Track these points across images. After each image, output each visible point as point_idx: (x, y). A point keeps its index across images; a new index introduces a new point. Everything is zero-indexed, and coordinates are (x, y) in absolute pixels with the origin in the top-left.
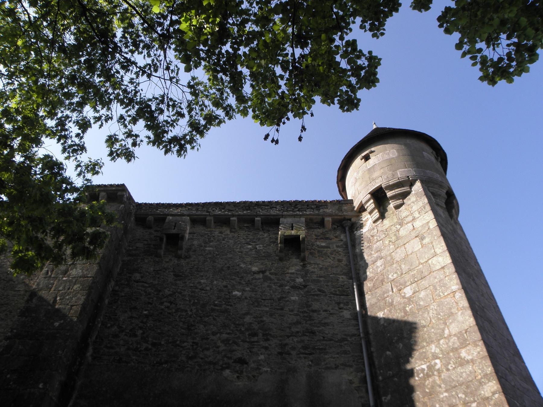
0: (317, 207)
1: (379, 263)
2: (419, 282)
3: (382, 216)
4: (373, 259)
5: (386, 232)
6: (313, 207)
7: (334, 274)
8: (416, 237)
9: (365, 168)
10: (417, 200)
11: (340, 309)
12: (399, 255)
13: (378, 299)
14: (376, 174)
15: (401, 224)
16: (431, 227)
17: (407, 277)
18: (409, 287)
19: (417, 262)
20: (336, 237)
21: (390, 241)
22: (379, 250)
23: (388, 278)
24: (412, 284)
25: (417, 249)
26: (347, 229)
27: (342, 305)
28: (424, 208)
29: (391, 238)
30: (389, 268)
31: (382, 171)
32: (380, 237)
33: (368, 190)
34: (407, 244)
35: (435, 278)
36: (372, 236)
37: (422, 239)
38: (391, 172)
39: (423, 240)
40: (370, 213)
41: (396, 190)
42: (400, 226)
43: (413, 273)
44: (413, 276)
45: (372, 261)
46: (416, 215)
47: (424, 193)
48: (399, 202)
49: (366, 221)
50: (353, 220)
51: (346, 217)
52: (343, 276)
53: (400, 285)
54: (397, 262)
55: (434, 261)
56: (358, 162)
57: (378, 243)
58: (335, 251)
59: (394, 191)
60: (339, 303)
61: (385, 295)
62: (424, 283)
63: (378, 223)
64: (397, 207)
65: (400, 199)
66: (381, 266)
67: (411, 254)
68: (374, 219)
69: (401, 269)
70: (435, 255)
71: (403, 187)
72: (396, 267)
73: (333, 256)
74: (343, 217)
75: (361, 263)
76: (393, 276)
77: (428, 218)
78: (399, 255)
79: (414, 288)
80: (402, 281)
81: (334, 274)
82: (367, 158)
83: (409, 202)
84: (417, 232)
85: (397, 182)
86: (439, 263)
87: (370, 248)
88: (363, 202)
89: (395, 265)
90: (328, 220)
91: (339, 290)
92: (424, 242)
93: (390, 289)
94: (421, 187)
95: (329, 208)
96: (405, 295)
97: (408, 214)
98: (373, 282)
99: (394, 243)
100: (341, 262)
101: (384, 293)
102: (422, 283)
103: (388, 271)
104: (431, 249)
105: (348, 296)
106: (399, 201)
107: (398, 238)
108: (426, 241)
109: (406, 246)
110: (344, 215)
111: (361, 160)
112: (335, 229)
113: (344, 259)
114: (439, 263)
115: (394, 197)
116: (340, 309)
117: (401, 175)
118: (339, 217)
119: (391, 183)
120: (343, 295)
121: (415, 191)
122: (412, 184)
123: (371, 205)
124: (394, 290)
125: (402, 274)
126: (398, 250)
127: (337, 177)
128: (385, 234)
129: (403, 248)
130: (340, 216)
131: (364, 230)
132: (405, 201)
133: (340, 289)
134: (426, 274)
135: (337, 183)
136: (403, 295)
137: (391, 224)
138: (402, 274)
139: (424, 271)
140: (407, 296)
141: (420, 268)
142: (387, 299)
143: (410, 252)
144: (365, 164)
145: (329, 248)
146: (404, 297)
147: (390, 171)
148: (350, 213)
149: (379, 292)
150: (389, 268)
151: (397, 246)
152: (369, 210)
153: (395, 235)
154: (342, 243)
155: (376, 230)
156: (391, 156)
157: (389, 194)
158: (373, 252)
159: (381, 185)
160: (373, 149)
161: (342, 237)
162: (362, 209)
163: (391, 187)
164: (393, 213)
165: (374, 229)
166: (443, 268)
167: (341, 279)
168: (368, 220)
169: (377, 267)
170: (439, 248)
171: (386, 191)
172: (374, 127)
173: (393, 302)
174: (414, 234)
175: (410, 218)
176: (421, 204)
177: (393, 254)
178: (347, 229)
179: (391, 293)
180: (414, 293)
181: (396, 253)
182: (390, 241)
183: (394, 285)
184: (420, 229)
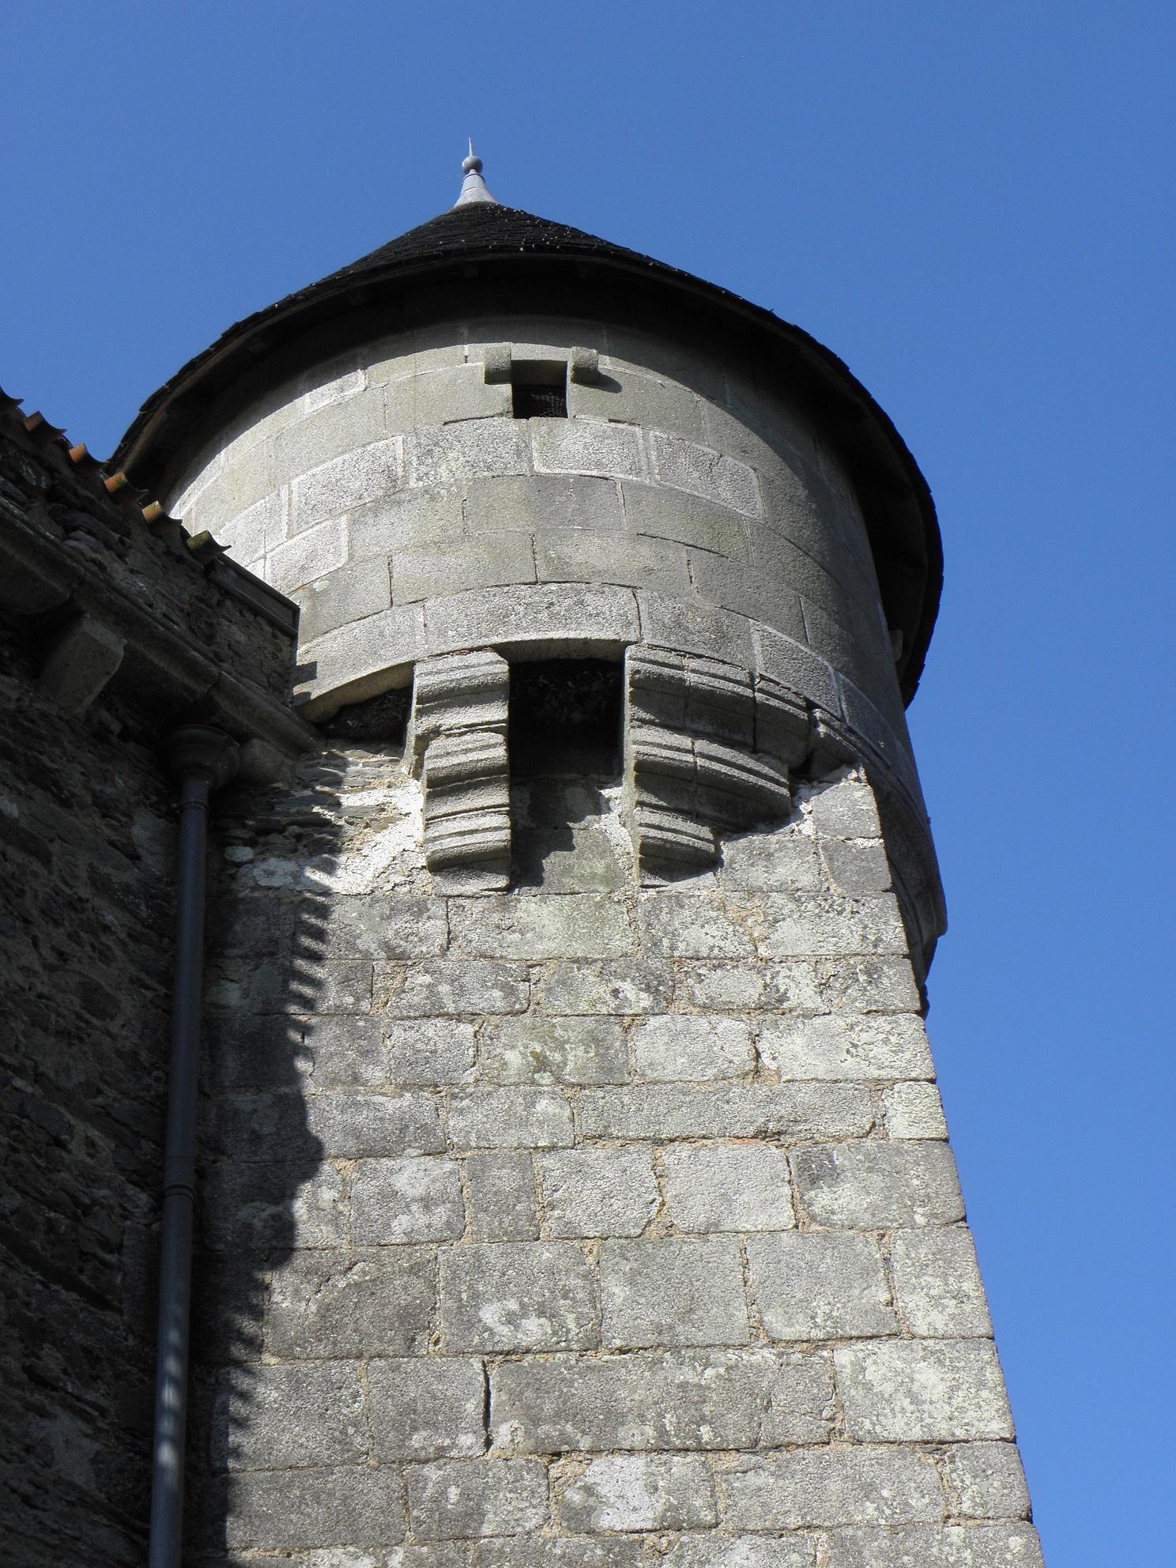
0: (51, 495)
1: (411, 1175)
2: (731, 1461)
3: (521, 862)
4: (362, 1118)
5: (522, 988)
6: (28, 472)
7: (38, 1078)
8: (762, 1134)
9: (507, 453)
10: (819, 893)
11: (40, 1381)
12: (598, 1190)
13: (344, 1441)
14: (589, 551)
15: (663, 992)
16: (900, 1126)
17: (635, 1385)
18: (638, 1463)
19: (741, 1315)
20: (104, 807)
21: (541, 1064)
22: (423, 1077)
23: (466, 1319)
24: (662, 1448)
25: (759, 1221)
26: (197, 792)
27: (51, 1360)
28: (873, 973)
29: (560, 1046)
30: (492, 1253)
31: (646, 553)
32: (461, 992)
33: (503, 617)
34: (684, 1150)
35: (869, 1490)
36: (397, 956)
37: (814, 1171)
38: (708, 606)
39: (814, 1181)
40: (442, 787)
41: (701, 745)
42: (646, 1001)
43: (687, 1375)
44: (691, 1397)
45: (355, 1133)
46: (801, 990)
47: (886, 879)
48: (691, 833)
49: (380, 818)
50: (263, 754)
51: (225, 705)
52: (95, 1134)
53: (558, 1416)
54: (570, 1235)
55: (882, 1363)
56: (455, 371)
57: (433, 1029)
58: (75, 904)
59: (685, 742)
60: (36, 1333)
61: (417, 1440)
62: (769, 1488)
63: (473, 886)
64: (664, 861)
65: (696, 817)
66: (427, 1203)
67: (703, 1234)
68: (452, 845)
69: (593, 1300)
70: (891, 1330)
71: (754, 751)
72: (551, 1271)
73: (59, 935)
74: (201, 689)
75: (244, 1101)
76: (511, 1319)
77: (881, 1052)
78: (598, 1190)
79: (679, 1489)
80: (583, 1390)
81: (38, 1078)
82: (535, 394)
83: (758, 876)
84: (783, 1109)
85: (738, 699)
86: (915, 1400)
87: (355, 1034)
88: (421, 682)
89: (545, 1254)
90: (101, 638)
91: (51, 1226)
92: (822, 1199)
93: (472, 1407)
94: (874, 827)
95: (135, 559)
96: (589, 1511)
97: (731, 947)
98: (327, 1295)
99: (572, 1090)
100: (103, 1015)
101: (409, 1418)
102: (753, 1480)
103: (478, 1265)
104: (867, 1273)
105: (105, 1305)
106: (690, 827)
107: (612, 1074)
108: (842, 1199)
109: (668, 1157)
110: (218, 684)
111: (493, 377)
112: (100, 736)
113: (128, 1004)
114: (915, 1400)
115: (658, 779)
116: (40, 1381)
117: (770, 662)
118: (176, 673)
119: (691, 678)
120: (72, 1285)
121: (820, 825)
122: (812, 767)
123: (476, 737)
124: (503, 1433)
125: (593, 1343)
126: (596, 1154)
127: (191, 366)
128: (509, 991)
129: (639, 1161)
130: (191, 667)
131: (349, 877)
132: (728, 850)
133: (63, 1224)
134: (800, 1429)
135: (150, 407)
136: (575, 1497)
137: (579, 949)
138: (593, 1343)
139: (781, 1398)
140: (608, 1520)
141: (760, 1371)
142: (432, 1472)
143: (698, 1214)
144: (514, 426)
145: (46, 860)
146: (579, 1520)
147: (706, 590)
148: (258, 696)
149: (364, 1387)
150: (492, 1253)
151: (592, 1125)
152: (445, 756)
153: (594, 1040)
154: (129, 876)
155: (434, 927)
156: (725, 493)
157: (642, 739)
158: (374, 1074)
159: (619, 647)
160: (607, 365)
161: (143, 828)
162: (378, 715)
163: (676, 704)
164: (612, 879)
165: (418, 909)
166: (936, 1446)
167: (77, 1151)
168: (390, 828)
169: (388, 1196)
170: (936, 1302)
171: (629, 710)
172: (471, 191)
173: (476, 1515)
174: (746, 1107)
175: (746, 987)
176: (848, 933)
177: (549, 1161)
178: (197, 792)
179: (468, 1440)
180: (670, 1524)
181: (580, 1169)
182: (541, 1064)
183: (515, 1396)
184: (805, 1095)
